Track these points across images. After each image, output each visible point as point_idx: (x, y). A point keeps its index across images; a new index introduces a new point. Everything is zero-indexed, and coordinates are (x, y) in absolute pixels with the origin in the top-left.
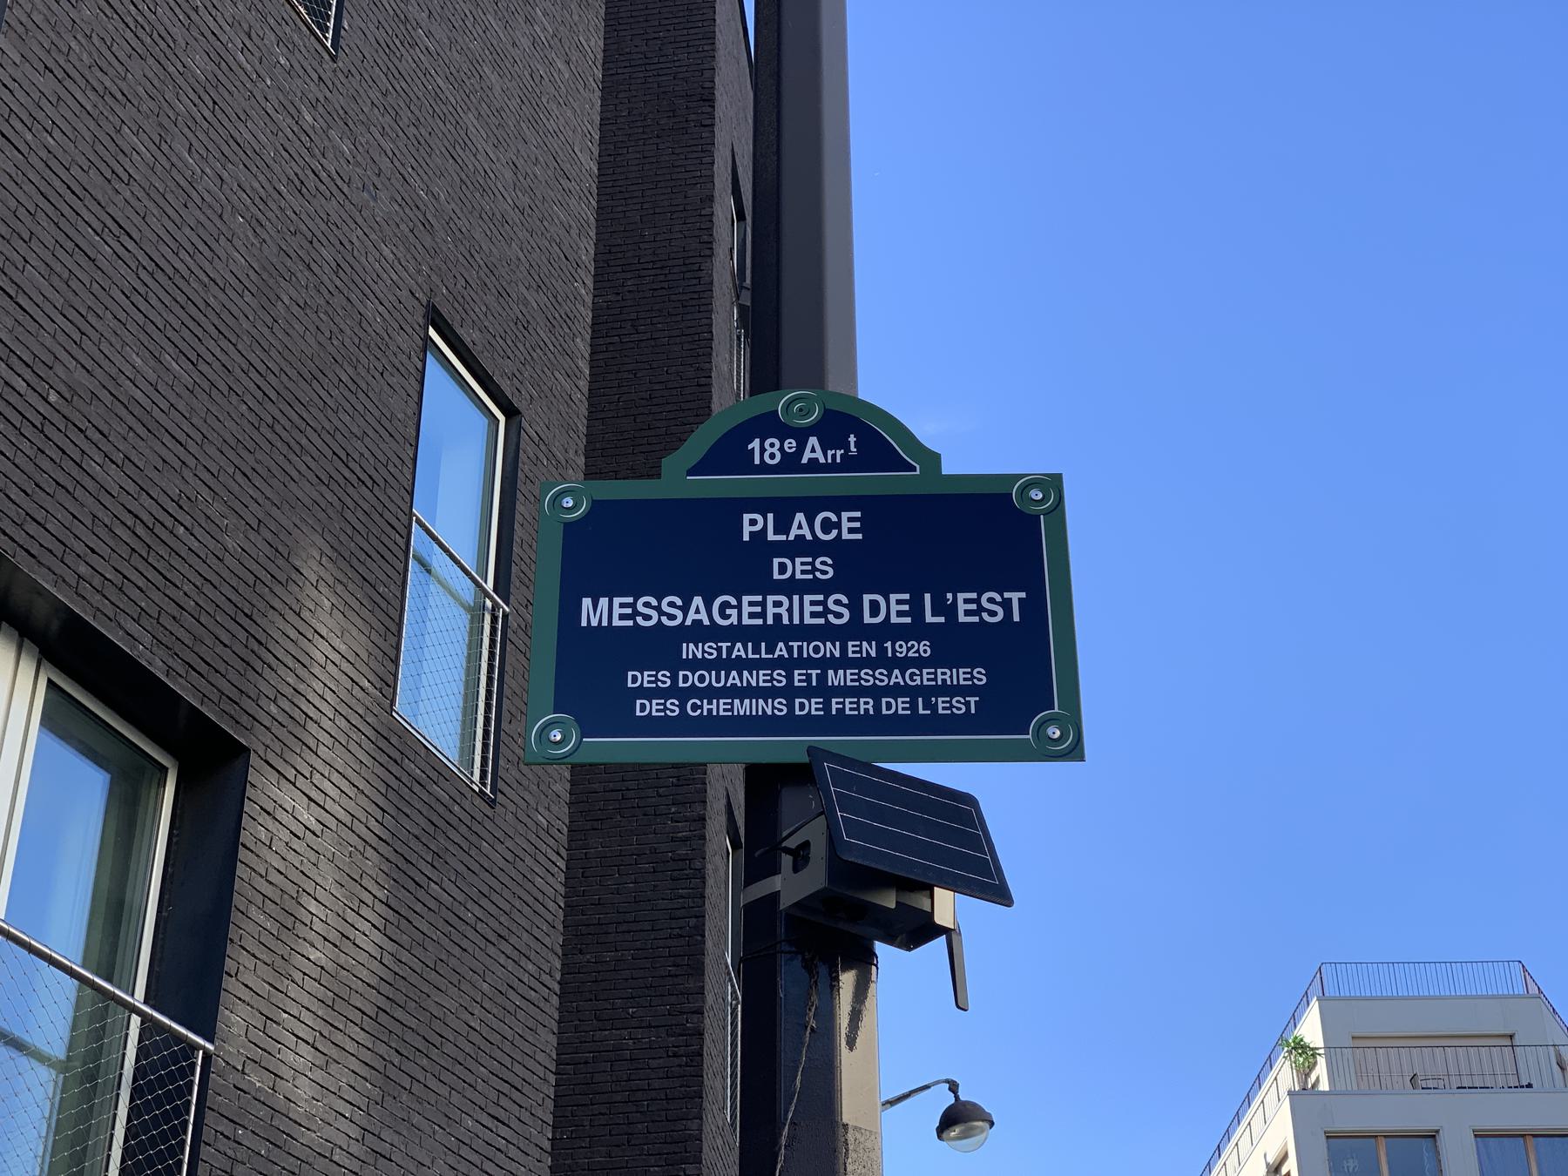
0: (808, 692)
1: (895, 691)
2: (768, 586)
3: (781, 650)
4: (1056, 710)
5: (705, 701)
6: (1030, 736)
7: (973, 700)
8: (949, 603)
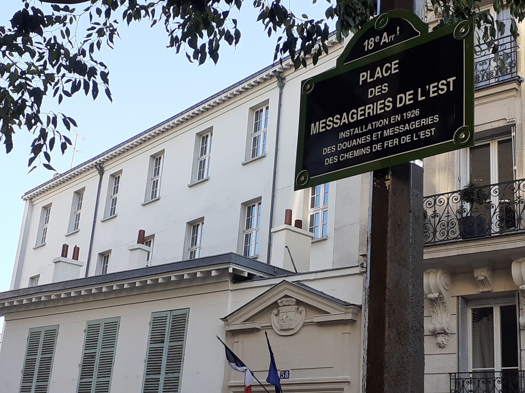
0: (376, 142)
1: (405, 133)
2: (365, 102)
3: (370, 127)
4: (464, 126)
5: (345, 154)
6: (453, 140)
7: (433, 129)
8: (427, 90)
